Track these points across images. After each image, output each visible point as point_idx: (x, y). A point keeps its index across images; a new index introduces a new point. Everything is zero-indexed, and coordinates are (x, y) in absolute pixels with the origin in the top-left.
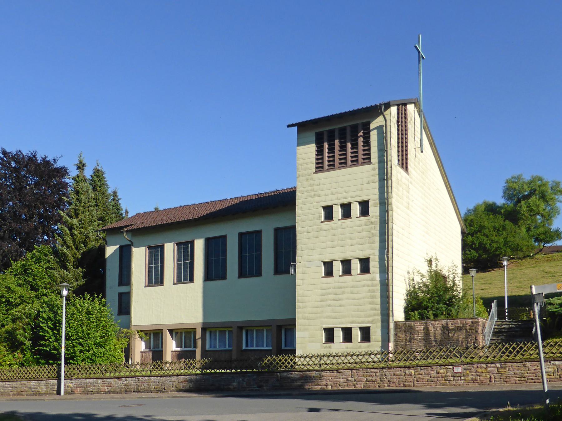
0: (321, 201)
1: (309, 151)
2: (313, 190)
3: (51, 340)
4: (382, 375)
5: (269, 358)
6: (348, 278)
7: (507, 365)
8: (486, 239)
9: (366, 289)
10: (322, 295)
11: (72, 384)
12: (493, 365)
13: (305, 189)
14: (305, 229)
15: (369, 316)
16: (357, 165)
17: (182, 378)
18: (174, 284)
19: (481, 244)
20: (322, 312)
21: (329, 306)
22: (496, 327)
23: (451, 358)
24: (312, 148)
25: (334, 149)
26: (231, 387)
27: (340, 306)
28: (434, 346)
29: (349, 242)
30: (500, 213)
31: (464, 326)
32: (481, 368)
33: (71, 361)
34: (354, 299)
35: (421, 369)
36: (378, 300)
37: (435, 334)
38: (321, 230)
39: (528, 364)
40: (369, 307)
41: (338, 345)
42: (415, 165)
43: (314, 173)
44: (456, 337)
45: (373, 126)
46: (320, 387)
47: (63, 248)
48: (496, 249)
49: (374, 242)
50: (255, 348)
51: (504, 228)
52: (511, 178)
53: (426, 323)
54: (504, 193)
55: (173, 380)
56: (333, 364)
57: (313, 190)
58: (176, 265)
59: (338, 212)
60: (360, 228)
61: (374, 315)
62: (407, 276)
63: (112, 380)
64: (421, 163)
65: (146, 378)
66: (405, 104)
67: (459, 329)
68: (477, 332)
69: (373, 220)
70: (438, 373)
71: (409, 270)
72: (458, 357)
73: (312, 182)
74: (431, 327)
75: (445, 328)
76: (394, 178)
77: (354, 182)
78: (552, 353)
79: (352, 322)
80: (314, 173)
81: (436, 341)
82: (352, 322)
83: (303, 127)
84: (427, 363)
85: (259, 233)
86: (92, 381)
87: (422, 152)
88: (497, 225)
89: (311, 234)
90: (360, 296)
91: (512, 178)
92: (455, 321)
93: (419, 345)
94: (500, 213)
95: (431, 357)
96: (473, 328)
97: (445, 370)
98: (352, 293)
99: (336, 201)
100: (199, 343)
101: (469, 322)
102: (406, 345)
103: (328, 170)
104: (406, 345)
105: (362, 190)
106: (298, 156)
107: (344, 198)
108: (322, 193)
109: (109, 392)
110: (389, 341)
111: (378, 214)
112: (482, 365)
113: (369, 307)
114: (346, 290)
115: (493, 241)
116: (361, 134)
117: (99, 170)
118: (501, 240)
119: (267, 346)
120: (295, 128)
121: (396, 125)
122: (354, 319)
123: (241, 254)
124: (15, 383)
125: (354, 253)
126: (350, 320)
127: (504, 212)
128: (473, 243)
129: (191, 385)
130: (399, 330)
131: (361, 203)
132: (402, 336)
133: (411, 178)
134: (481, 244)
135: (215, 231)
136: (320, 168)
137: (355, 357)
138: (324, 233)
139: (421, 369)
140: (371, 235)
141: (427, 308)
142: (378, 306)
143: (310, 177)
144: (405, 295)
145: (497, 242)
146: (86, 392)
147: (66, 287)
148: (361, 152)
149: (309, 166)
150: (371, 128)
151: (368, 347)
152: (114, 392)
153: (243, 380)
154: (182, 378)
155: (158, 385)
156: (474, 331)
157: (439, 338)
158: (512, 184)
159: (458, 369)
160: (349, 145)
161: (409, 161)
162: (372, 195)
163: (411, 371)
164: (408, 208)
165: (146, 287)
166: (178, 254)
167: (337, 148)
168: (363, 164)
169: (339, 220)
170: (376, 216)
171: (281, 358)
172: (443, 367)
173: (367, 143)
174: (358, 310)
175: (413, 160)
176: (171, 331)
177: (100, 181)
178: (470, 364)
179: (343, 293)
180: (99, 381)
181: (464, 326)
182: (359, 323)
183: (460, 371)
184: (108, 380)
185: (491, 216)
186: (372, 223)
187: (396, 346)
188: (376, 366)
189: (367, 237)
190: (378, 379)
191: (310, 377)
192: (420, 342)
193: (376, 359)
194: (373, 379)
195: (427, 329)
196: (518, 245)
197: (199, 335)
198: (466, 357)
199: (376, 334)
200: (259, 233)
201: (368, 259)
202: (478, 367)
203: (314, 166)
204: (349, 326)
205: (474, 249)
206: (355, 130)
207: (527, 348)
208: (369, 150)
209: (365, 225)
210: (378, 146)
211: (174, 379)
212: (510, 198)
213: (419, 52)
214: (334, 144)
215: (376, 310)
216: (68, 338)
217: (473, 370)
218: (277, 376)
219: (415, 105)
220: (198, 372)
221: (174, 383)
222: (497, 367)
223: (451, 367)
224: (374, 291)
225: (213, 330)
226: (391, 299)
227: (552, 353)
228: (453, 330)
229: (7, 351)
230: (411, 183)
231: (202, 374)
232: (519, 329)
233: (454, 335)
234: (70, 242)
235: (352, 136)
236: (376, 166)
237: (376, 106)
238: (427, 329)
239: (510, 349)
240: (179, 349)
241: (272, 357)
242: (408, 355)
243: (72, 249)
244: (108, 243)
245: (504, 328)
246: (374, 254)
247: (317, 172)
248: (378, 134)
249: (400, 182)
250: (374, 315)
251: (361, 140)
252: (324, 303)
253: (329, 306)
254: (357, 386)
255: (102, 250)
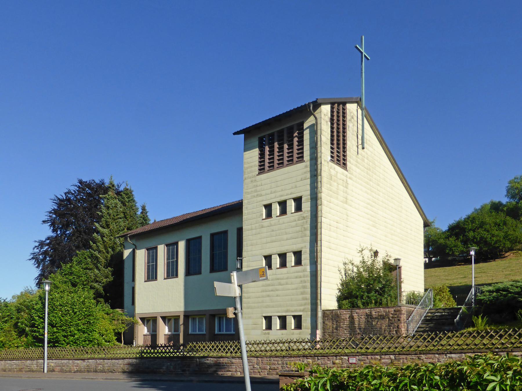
0: (262, 201)
1: (252, 156)
2: (256, 191)
3: (39, 327)
4: (283, 364)
5: (191, 344)
6: (284, 270)
7: (401, 357)
8: (487, 234)
9: (299, 280)
10: (263, 286)
11: (53, 363)
12: (387, 357)
13: (249, 190)
14: (249, 227)
15: (301, 305)
16: (292, 164)
17: (126, 361)
18: (165, 279)
19: (482, 238)
20: (263, 302)
21: (268, 296)
22: (429, 314)
23: (347, 348)
24: (256, 152)
25: (273, 151)
26: (161, 370)
27: (277, 296)
28: (359, 333)
29: (285, 237)
30: (502, 211)
31: (387, 315)
32: (375, 359)
33: (56, 345)
34: (289, 290)
35: (318, 359)
36: (309, 290)
37: (359, 322)
38: (262, 227)
39: (423, 357)
40: (301, 297)
41: (276, 333)
42: (357, 162)
43: (257, 175)
44: (379, 325)
45: (306, 125)
46: (231, 373)
47: (95, 253)
48: (496, 242)
49: (305, 236)
50: (224, 333)
51: (505, 224)
52: (513, 178)
53: (351, 312)
54: (508, 191)
55: (120, 363)
56: (277, 351)
57: (256, 191)
58: (166, 263)
59: (276, 209)
60: (294, 224)
61: (305, 304)
62: (342, 267)
63: (79, 362)
64: (366, 160)
65: (102, 361)
66: (344, 104)
67: (382, 317)
68: (399, 320)
69: (305, 215)
70: (334, 363)
71: (339, 261)
72: (354, 348)
73: (255, 184)
74: (355, 315)
75: (369, 316)
76: (323, 174)
77: (290, 179)
78: (450, 345)
79: (287, 311)
80: (257, 175)
81: (360, 329)
82: (287, 311)
83: (248, 132)
84: (337, 352)
85: (225, 233)
86: (65, 361)
87: (363, 148)
88: (498, 221)
89: (254, 231)
90: (294, 286)
91: (515, 178)
92: (378, 310)
93: (344, 334)
94: (502, 211)
95: (334, 346)
96: (396, 316)
97: (340, 361)
98: (287, 284)
99: (274, 199)
100: (182, 328)
101: (392, 310)
102: (333, 332)
103: (269, 171)
104: (333, 332)
105: (296, 187)
106: (245, 161)
107: (282, 196)
108: (263, 193)
109: (77, 371)
110: (316, 328)
111: (309, 209)
112: (376, 356)
113: (301, 297)
114: (283, 282)
115: (493, 236)
116: (296, 134)
117: (127, 189)
118: (502, 234)
119: (226, 331)
120: (242, 136)
121: (329, 123)
122: (288, 308)
123: (213, 251)
124: (17, 362)
125: (289, 246)
126: (285, 309)
127: (507, 209)
128: (474, 237)
129: (130, 368)
130: (326, 318)
131: (295, 200)
132: (329, 324)
133: (352, 174)
134: (482, 238)
135: (193, 233)
136: (262, 170)
137: (260, 346)
138: (264, 230)
139: (318, 359)
140: (303, 229)
141: (357, 297)
142: (309, 296)
143: (254, 179)
144: (339, 285)
145: (497, 236)
146: (62, 371)
147: (48, 283)
148: (295, 151)
149: (253, 169)
150: (304, 128)
151: (300, 334)
152: (80, 371)
153: (171, 365)
154: (126, 361)
155: (109, 367)
156: (396, 319)
157: (363, 326)
158: (514, 184)
159: (353, 360)
160: (286, 146)
161: (348, 158)
162: (304, 191)
163: (309, 360)
164: (346, 203)
165: (145, 281)
166: (167, 254)
167: (276, 150)
168: (297, 162)
169: (277, 217)
170: (308, 211)
171: (200, 344)
172: (338, 357)
173: (301, 142)
174: (292, 300)
175: (354, 157)
176: (164, 318)
177: (128, 198)
178: (364, 355)
179: (280, 284)
180: (71, 361)
181: (387, 315)
182: (292, 312)
183: (354, 361)
184: (76, 361)
185: (493, 213)
186: (304, 218)
187: (324, 333)
188: (278, 354)
189: (299, 231)
190: (280, 367)
191: (223, 363)
192: (345, 329)
193: (306, 347)
194: (275, 367)
195: (352, 318)
196: (517, 237)
197: (181, 321)
198: (361, 348)
199: (306, 322)
200: (225, 233)
201: (301, 252)
202: (372, 359)
203: (257, 168)
204: (284, 314)
205: (476, 243)
206: (291, 131)
207: (386, 340)
208: (303, 149)
209: (299, 220)
210: (310, 144)
211: (121, 361)
212: (513, 197)
213: (362, 53)
214: (273, 147)
215: (306, 299)
216: (51, 325)
217: (368, 361)
218: (196, 361)
219: (358, 105)
220: (138, 356)
221: (121, 366)
222: (391, 359)
223: (346, 358)
224: (305, 282)
225: (194, 317)
226: (319, 289)
227: (450, 345)
228: (376, 318)
229: (17, 335)
230: (350, 178)
231: (139, 358)
232: (450, 317)
233: (377, 324)
234: (102, 248)
235: (289, 137)
236: (308, 163)
237: (305, 105)
238: (352, 318)
239: (429, 339)
240: (170, 333)
241: (193, 344)
242: (337, 343)
243: (103, 253)
244: (137, 247)
245: (436, 316)
246: (305, 247)
247: (259, 174)
248: (310, 133)
249: (333, 177)
250: (305, 304)
251: (296, 139)
252: (264, 294)
253: (268, 296)
254: (261, 373)
255: (121, 254)
